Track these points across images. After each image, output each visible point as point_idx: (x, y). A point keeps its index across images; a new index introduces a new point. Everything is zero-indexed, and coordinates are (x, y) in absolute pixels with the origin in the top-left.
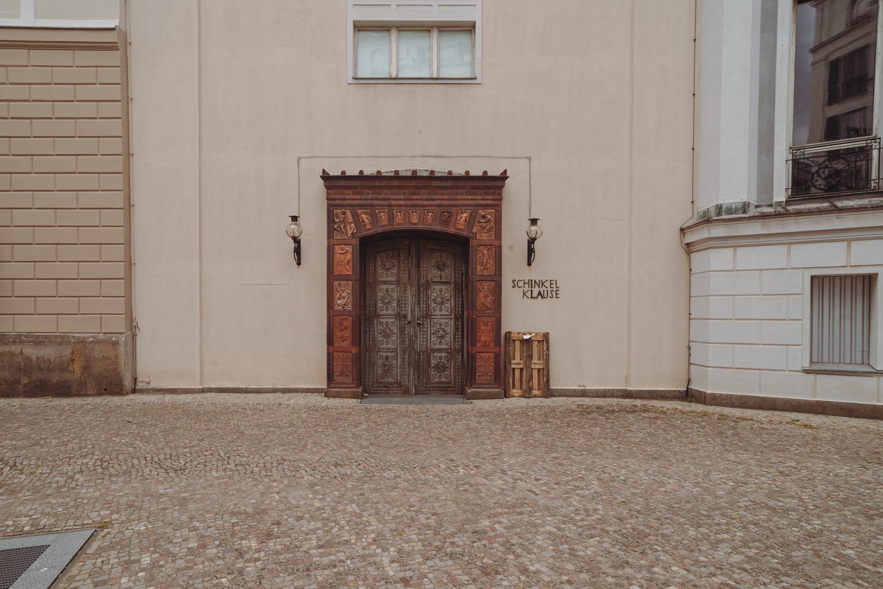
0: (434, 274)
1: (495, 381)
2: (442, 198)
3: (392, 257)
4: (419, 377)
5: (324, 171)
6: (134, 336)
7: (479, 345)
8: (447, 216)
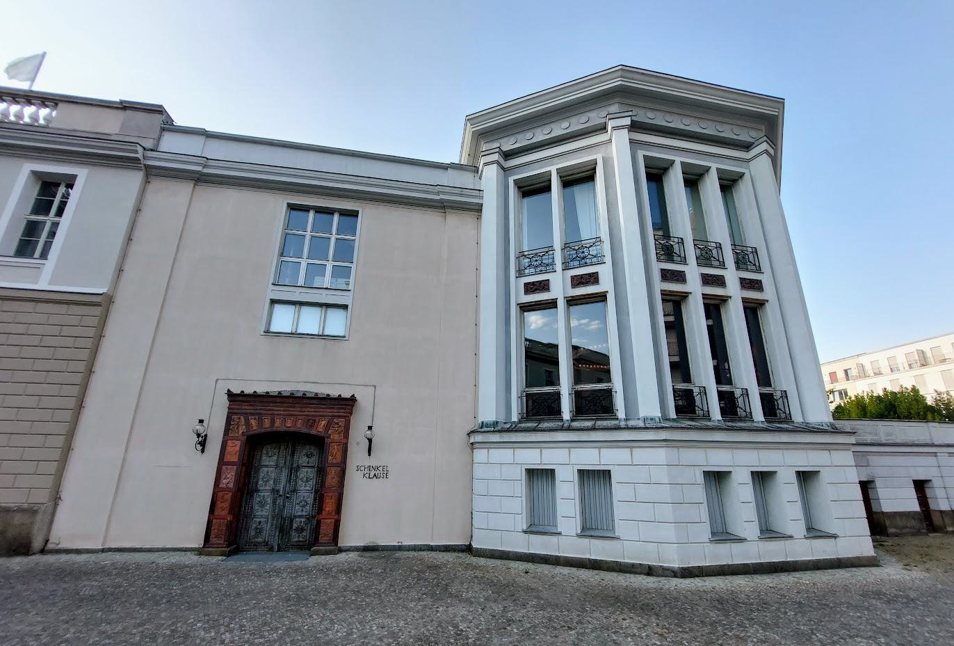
0: (303, 460)
1: (333, 541)
2: (310, 411)
3: (275, 449)
4: (282, 538)
5: (229, 390)
6: (56, 505)
7: (324, 513)
8: (312, 423)
